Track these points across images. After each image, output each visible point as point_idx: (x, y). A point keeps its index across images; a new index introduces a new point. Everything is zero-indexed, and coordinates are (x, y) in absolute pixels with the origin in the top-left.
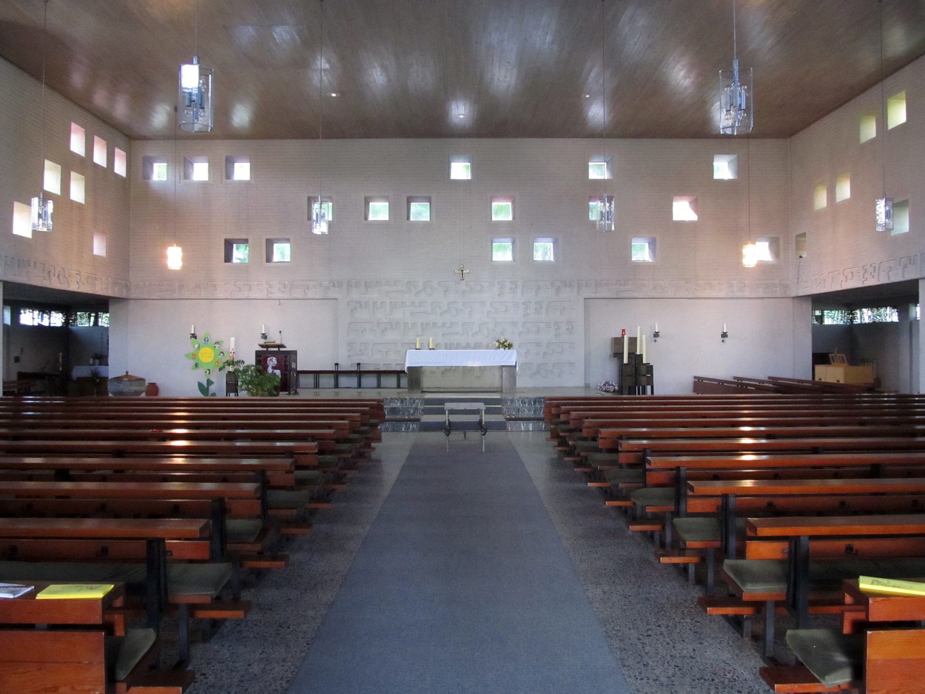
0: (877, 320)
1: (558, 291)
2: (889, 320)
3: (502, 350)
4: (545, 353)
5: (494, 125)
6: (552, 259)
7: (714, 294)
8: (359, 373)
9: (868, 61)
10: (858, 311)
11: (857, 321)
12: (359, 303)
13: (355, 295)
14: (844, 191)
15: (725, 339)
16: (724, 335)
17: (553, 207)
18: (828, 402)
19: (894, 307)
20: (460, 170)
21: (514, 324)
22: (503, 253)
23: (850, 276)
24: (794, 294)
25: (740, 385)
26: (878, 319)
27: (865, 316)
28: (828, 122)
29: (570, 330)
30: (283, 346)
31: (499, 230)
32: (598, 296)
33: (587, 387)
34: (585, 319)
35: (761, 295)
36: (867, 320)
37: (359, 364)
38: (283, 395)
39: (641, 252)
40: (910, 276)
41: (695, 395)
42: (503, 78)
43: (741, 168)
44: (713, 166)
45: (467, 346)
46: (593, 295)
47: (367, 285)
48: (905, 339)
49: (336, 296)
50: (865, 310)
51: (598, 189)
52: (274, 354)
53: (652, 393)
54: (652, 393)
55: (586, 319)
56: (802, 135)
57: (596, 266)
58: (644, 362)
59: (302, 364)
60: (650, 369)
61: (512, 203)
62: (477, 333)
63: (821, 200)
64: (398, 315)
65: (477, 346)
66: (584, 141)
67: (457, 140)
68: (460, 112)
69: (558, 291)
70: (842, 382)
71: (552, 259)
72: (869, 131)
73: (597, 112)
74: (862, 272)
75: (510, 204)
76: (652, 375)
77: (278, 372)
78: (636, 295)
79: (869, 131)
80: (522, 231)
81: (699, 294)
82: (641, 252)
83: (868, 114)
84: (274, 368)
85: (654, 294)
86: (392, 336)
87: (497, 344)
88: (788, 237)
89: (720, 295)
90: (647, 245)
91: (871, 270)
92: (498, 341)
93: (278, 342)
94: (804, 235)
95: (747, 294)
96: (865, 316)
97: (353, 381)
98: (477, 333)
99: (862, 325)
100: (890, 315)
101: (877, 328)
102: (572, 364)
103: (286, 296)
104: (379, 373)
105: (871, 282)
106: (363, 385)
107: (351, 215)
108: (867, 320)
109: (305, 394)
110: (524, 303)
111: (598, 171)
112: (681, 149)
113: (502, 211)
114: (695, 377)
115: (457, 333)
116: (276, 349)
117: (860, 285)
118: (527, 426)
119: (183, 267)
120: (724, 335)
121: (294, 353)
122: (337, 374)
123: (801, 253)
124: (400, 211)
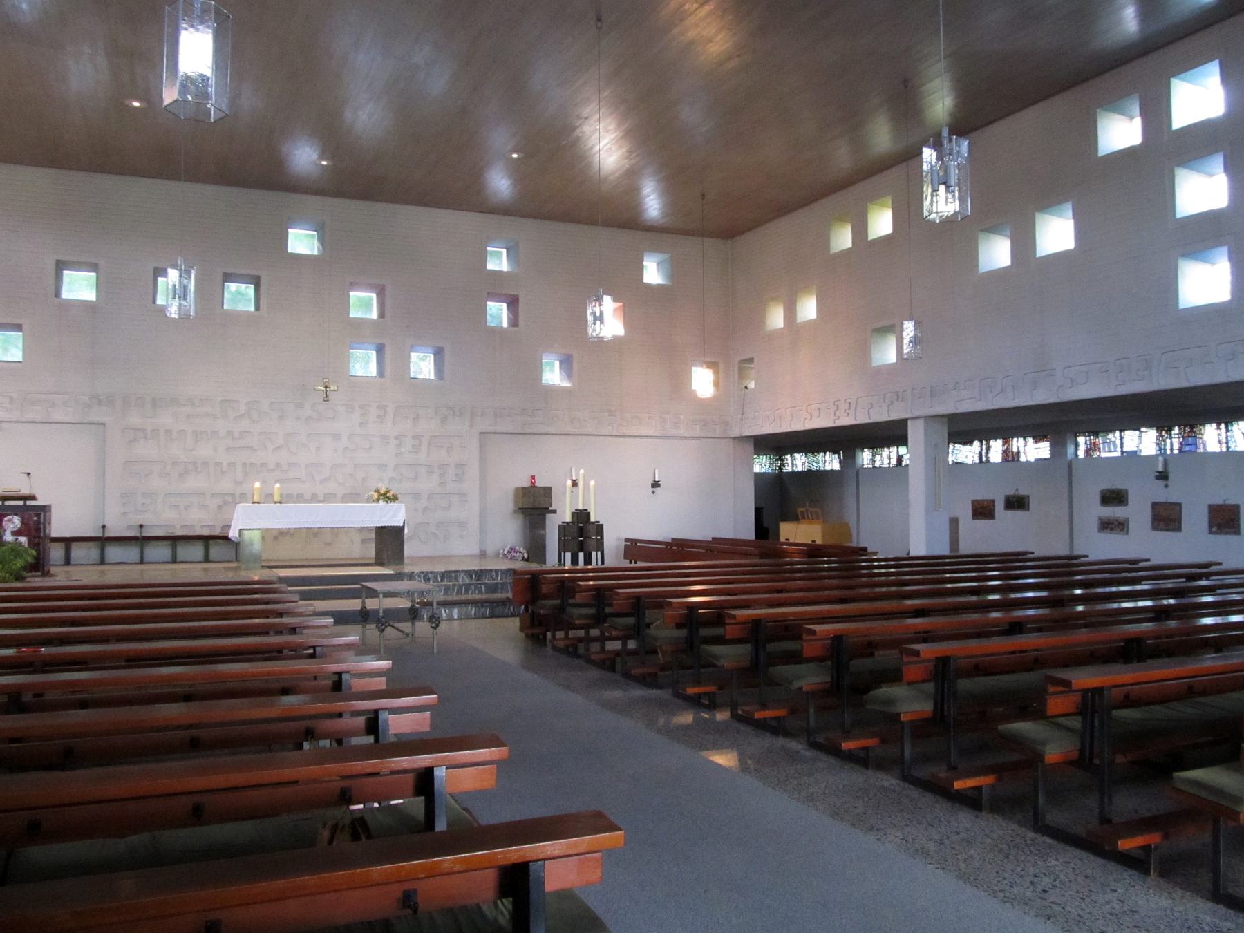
0: (813, 468)
1: (444, 420)
2: (828, 468)
3: (382, 503)
4: (425, 509)
5: (359, 181)
6: (432, 377)
7: (644, 431)
8: (141, 540)
9: (842, 158)
10: (788, 457)
11: (788, 469)
12: (143, 430)
13: (134, 419)
14: (808, 309)
15: (657, 490)
16: (656, 485)
17: (432, 305)
18: (800, 571)
19: (835, 452)
20: (302, 241)
21: (382, 467)
22: (364, 364)
23: (816, 413)
24: (737, 434)
25: (678, 549)
26: (814, 467)
27: (798, 462)
28: (785, 225)
29: (460, 478)
30: (33, 498)
31: (357, 331)
32: (499, 429)
33: (483, 555)
34: (481, 459)
35: (697, 434)
36: (799, 468)
37: (141, 526)
38: (37, 581)
39: (553, 375)
40: (895, 416)
41: (626, 564)
42: (367, 116)
43: (674, 270)
44: (642, 267)
45: (314, 498)
46: (491, 429)
47: (155, 403)
48: (850, 490)
49: (103, 419)
50: (797, 456)
51: (496, 286)
52: (15, 510)
53: (603, 563)
54: (603, 563)
55: (483, 460)
56: (749, 237)
57: (496, 391)
58: (592, 519)
59: (59, 526)
60: (599, 528)
61: (378, 295)
62: (327, 480)
63: (776, 318)
64: (205, 451)
65: (329, 498)
66: (478, 218)
67: (304, 197)
68: (305, 157)
69: (444, 420)
70: (819, 542)
71: (432, 377)
72: (843, 239)
73: (500, 184)
74: (834, 408)
75: (374, 296)
76: (602, 538)
77: (23, 539)
78: (546, 429)
79: (843, 239)
80: (387, 339)
81: (625, 430)
82: (553, 375)
83: (842, 219)
84: (16, 533)
85: (569, 429)
86: (194, 482)
87: (376, 496)
88: (734, 364)
89: (651, 433)
90: (557, 363)
91: (844, 406)
92: (377, 491)
93: (25, 491)
94: (751, 360)
95: (682, 432)
96: (798, 462)
97: (132, 553)
98: (327, 480)
99: (794, 474)
100: (830, 462)
101: (812, 477)
102: (462, 524)
103: (14, 416)
104: (174, 540)
105: (846, 421)
106: (179, 558)
107: (126, 291)
108: (799, 468)
109: (60, 576)
110: (396, 438)
111: (498, 261)
112: (605, 240)
113: (363, 304)
114: (627, 540)
115: (299, 479)
116: (21, 503)
117: (831, 424)
118: (451, 612)
119: (1230, 104)
120: (656, 485)
121: (45, 509)
122: (103, 541)
123: (746, 383)
124: (209, 295)
